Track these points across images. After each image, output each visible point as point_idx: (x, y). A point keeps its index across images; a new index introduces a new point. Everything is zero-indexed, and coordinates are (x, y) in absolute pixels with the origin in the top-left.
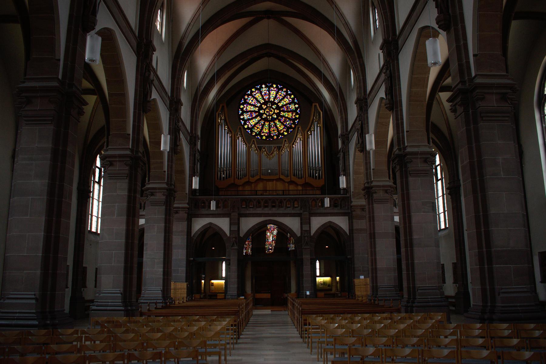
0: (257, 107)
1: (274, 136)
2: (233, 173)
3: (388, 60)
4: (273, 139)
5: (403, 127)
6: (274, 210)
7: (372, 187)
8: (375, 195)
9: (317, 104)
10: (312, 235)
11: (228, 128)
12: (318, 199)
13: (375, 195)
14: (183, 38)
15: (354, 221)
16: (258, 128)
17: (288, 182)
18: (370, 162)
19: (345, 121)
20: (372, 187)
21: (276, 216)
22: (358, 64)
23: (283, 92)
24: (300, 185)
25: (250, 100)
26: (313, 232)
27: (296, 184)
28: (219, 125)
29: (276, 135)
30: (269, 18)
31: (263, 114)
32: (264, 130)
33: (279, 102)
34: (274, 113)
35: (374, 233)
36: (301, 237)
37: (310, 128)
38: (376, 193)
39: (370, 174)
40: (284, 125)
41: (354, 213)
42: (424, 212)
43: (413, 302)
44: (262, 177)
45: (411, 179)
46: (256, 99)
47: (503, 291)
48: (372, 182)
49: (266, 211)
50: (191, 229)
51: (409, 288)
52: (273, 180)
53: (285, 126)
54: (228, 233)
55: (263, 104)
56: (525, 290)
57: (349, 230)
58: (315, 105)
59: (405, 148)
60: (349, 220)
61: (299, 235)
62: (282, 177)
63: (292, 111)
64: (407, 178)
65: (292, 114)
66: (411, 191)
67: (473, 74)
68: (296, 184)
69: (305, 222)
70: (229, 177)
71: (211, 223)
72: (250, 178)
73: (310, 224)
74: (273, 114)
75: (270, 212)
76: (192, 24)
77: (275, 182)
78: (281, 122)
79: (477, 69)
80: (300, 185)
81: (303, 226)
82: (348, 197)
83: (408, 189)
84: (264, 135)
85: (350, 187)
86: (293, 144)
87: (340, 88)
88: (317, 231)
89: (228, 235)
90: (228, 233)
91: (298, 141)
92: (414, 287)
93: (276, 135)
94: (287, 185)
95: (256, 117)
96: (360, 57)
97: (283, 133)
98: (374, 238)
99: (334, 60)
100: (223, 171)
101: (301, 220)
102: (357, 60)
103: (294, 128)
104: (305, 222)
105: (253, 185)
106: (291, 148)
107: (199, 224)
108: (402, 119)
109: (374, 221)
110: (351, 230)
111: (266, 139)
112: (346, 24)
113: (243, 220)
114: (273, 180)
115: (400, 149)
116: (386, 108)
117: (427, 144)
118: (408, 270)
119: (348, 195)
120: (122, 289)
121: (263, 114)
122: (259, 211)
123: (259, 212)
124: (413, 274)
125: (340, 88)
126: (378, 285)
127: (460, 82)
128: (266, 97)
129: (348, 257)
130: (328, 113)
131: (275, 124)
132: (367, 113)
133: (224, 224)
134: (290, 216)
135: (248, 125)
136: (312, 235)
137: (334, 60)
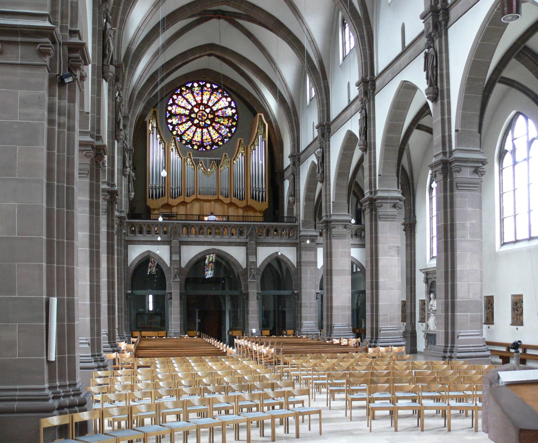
0: (188, 110)
1: (207, 146)
2: (166, 190)
3: (364, 100)
4: (206, 149)
5: (375, 170)
6: (218, 239)
7: (331, 222)
8: (333, 230)
9: (262, 115)
10: (258, 267)
11: (161, 138)
12: (264, 227)
13: (333, 230)
14: (131, 43)
15: (303, 252)
16: (188, 135)
17: (227, 204)
18: (330, 194)
19: (296, 141)
20: (331, 222)
21: (221, 245)
22: (322, 86)
23: (218, 94)
24: (241, 208)
25: (180, 101)
26: (259, 264)
27: (237, 207)
28: (150, 134)
29: (209, 145)
30: (219, 18)
31: (194, 119)
32: (180, 127)
33: (214, 105)
34: (208, 118)
35: (331, 270)
36: (246, 269)
37: (254, 143)
38: (334, 227)
39: (330, 208)
40: (218, 133)
41: (302, 244)
42: (389, 256)
43: (376, 342)
44: (199, 197)
45: (380, 223)
46: (187, 100)
47: (461, 334)
48: (330, 216)
49: (210, 238)
50: (127, 258)
51: (372, 328)
52: (210, 201)
53: (220, 134)
54: (168, 263)
55: (195, 106)
56: (477, 333)
57: (297, 262)
58: (260, 116)
59: (376, 192)
60: (297, 251)
61: (244, 266)
62: (221, 197)
63: (228, 118)
64: (376, 221)
65: (228, 121)
66: (380, 235)
67: (454, 148)
68: (237, 207)
69: (251, 252)
70: (162, 196)
71: (149, 252)
72: (186, 197)
73: (256, 255)
74: (206, 120)
75: (213, 240)
76: (142, 28)
77: (213, 202)
78: (215, 130)
79: (458, 144)
80: (241, 208)
81: (249, 256)
82: (297, 226)
83: (376, 233)
84: (196, 144)
85: (300, 214)
86: (234, 160)
87: (293, 102)
88: (263, 262)
89: (169, 265)
90: (168, 263)
91: (240, 156)
92: (377, 328)
93: (209, 145)
94: (226, 207)
95: (186, 122)
96: (325, 78)
97: (217, 143)
98: (331, 275)
99: (287, 68)
100: (156, 189)
101: (247, 249)
102: (322, 81)
103: (230, 138)
104: (251, 252)
105: (188, 206)
106: (231, 163)
107: (136, 252)
108: (375, 162)
109: (331, 257)
110: (299, 263)
111: (198, 149)
112: (312, 41)
113: (184, 248)
114: (210, 201)
115: (371, 193)
116: (360, 149)
117: (397, 189)
118: (372, 311)
119: (297, 224)
120: (107, 330)
121: (194, 119)
122: (201, 238)
123: (202, 240)
124: (377, 316)
125: (293, 102)
126: (334, 323)
127: (443, 152)
128: (199, 98)
129: (296, 292)
130: (274, 124)
131: (209, 132)
132: (329, 141)
133: (162, 252)
134: (235, 246)
135: (177, 131)
136: (258, 267)
137: (287, 68)
